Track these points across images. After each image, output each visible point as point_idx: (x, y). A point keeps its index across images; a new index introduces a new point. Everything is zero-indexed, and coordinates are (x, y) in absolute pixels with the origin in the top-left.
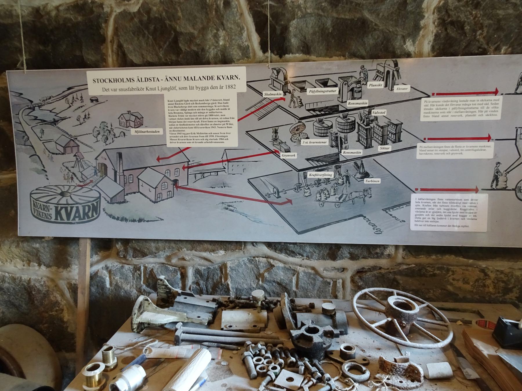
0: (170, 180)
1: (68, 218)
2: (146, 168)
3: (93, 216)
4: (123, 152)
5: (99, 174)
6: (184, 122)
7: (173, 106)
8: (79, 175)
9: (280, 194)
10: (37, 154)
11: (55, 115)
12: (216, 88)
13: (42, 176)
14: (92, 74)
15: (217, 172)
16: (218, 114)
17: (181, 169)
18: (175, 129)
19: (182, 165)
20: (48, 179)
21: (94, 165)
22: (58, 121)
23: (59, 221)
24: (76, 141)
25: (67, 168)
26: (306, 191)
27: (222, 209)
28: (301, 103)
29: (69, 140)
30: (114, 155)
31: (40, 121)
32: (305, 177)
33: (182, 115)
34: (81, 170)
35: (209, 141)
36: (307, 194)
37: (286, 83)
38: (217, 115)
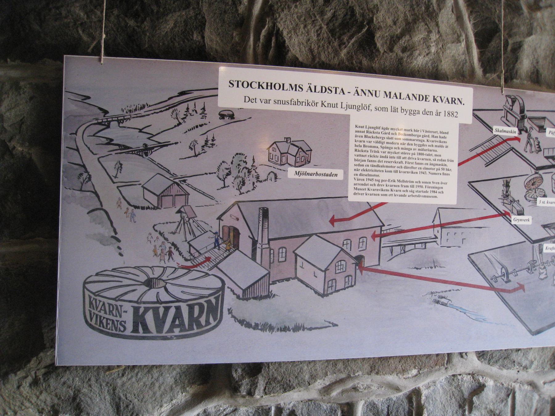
0: (351, 256)
1: (159, 328)
2: (310, 236)
3: (208, 322)
4: (271, 207)
5: (223, 246)
6: (379, 161)
7: (363, 134)
8: (184, 248)
9: (511, 277)
10: (104, 208)
11: (149, 138)
12: (431, 113)
13: (111, 250)
14: (225, 72)
15: (426, 243)
16: (431, 153)
17: (370, 239)
18: (364, 173)
19: (371, 231)
20: (121, 255)
21: (215, 229)
22: (153, 148)
23: (141, 333)
24: (184, 186)
25: (161, 234)
26: (542, 271)
27: (430, 304)
28: (539, 147)
29: (171, 183)
30: (253, 213)
31: (117, 147)
32: (541, 251)
33: (376, 149)
34: (189, 237)
35: (415, 194)
36: (542, 276)
37: (523, 118)
38: (429, 155)
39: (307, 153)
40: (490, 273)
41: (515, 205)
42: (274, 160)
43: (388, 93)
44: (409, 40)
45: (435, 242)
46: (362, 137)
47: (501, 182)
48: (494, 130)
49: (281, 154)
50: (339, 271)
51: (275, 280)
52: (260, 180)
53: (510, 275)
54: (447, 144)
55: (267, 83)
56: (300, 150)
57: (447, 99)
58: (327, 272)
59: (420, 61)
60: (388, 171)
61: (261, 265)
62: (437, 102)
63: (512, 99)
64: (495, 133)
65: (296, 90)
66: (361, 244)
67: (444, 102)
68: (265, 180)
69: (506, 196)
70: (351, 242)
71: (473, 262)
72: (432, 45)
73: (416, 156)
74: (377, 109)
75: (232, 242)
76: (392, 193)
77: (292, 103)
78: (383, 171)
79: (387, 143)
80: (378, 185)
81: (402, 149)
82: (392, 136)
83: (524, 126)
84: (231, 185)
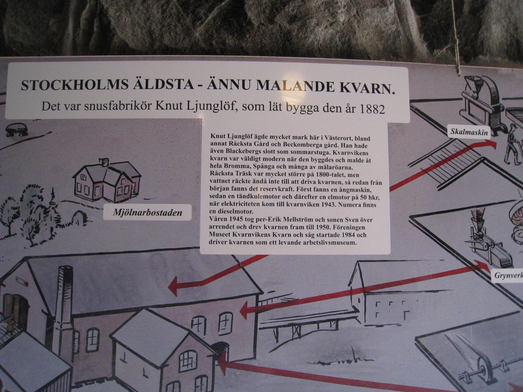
0: (205, 344)
2: (137, 310)
4: (77, 265)
6: (251, 189)
7: (224, 148)
9: (497, 373)
12: (338, 109)
15: (337, 320)
16: (340, 172)
17: (237, 316)
18: (225, 208)
30: (49, 274)
33: (246, 170)
35: (316, 239)
37: (498, 110)
39: (133, 180)
40: (457, 368)
41: (495, 250)
42: (83, 194)
43: (263, 83)
44: (300, 6)
45: (355, 317)
46: (222, 151)
47: (468, 214)
48: (449, 131)
49: (94, 183)
50: (185, 368)
51: (80, 380)
52: (61, 224)
53: (494, 371)
54: (369, 157)
55: (76, 81)
56: (123, 177)
57: (365, 86)
58: (165, 369)
59: (321, 34)
60: (267, 205)
61: (59, 356)
62: (348, 91)
63: (475, 81)
64: (450, 136)
65: (117, 88)
66: (222, 324)
67: (359, 90)
68: (69, 224)
69: (479, 236)
70: (205, 320)
71: (424, 350)
72: (340, 11)
73: (315, 178)
74: (245, 107)
75: (17, 320)
76: (275, 239)
77: (112, 106)
78: (258, 204)
79: (265, 159)
80: (251, 227)
81: (290, 167)
82: (274, 148)
83: (501, 123)
84: (19, 232)
